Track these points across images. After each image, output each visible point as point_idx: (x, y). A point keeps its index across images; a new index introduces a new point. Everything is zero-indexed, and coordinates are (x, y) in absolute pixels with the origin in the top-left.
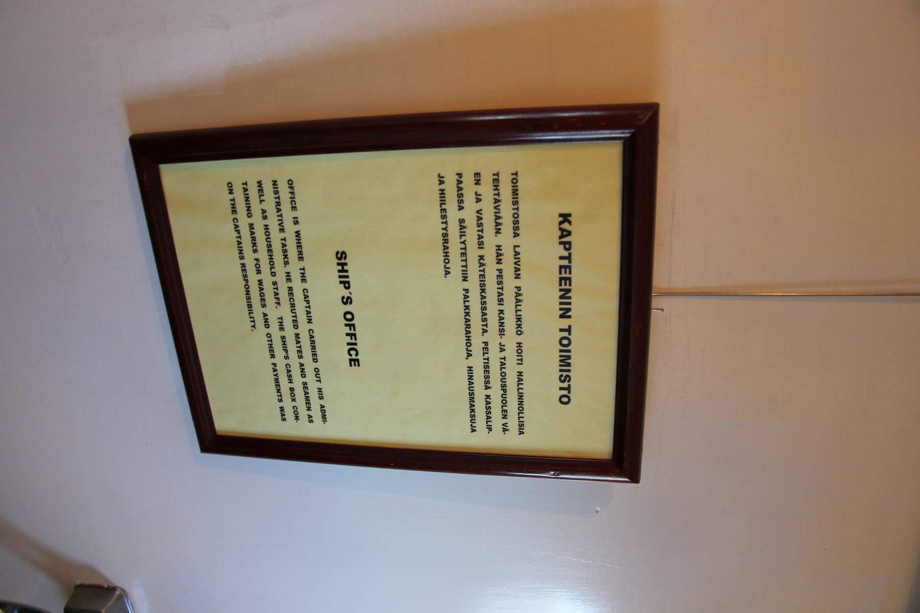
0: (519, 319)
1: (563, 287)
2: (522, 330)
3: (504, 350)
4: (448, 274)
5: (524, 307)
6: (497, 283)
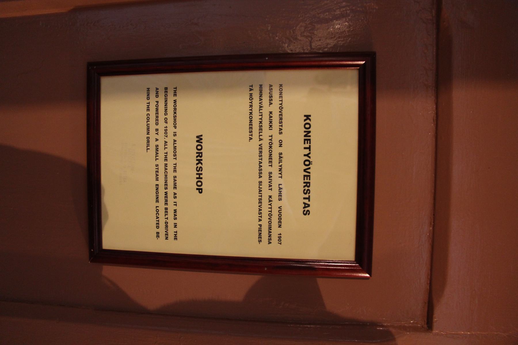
4: (271, 104)
6: (279, 200)
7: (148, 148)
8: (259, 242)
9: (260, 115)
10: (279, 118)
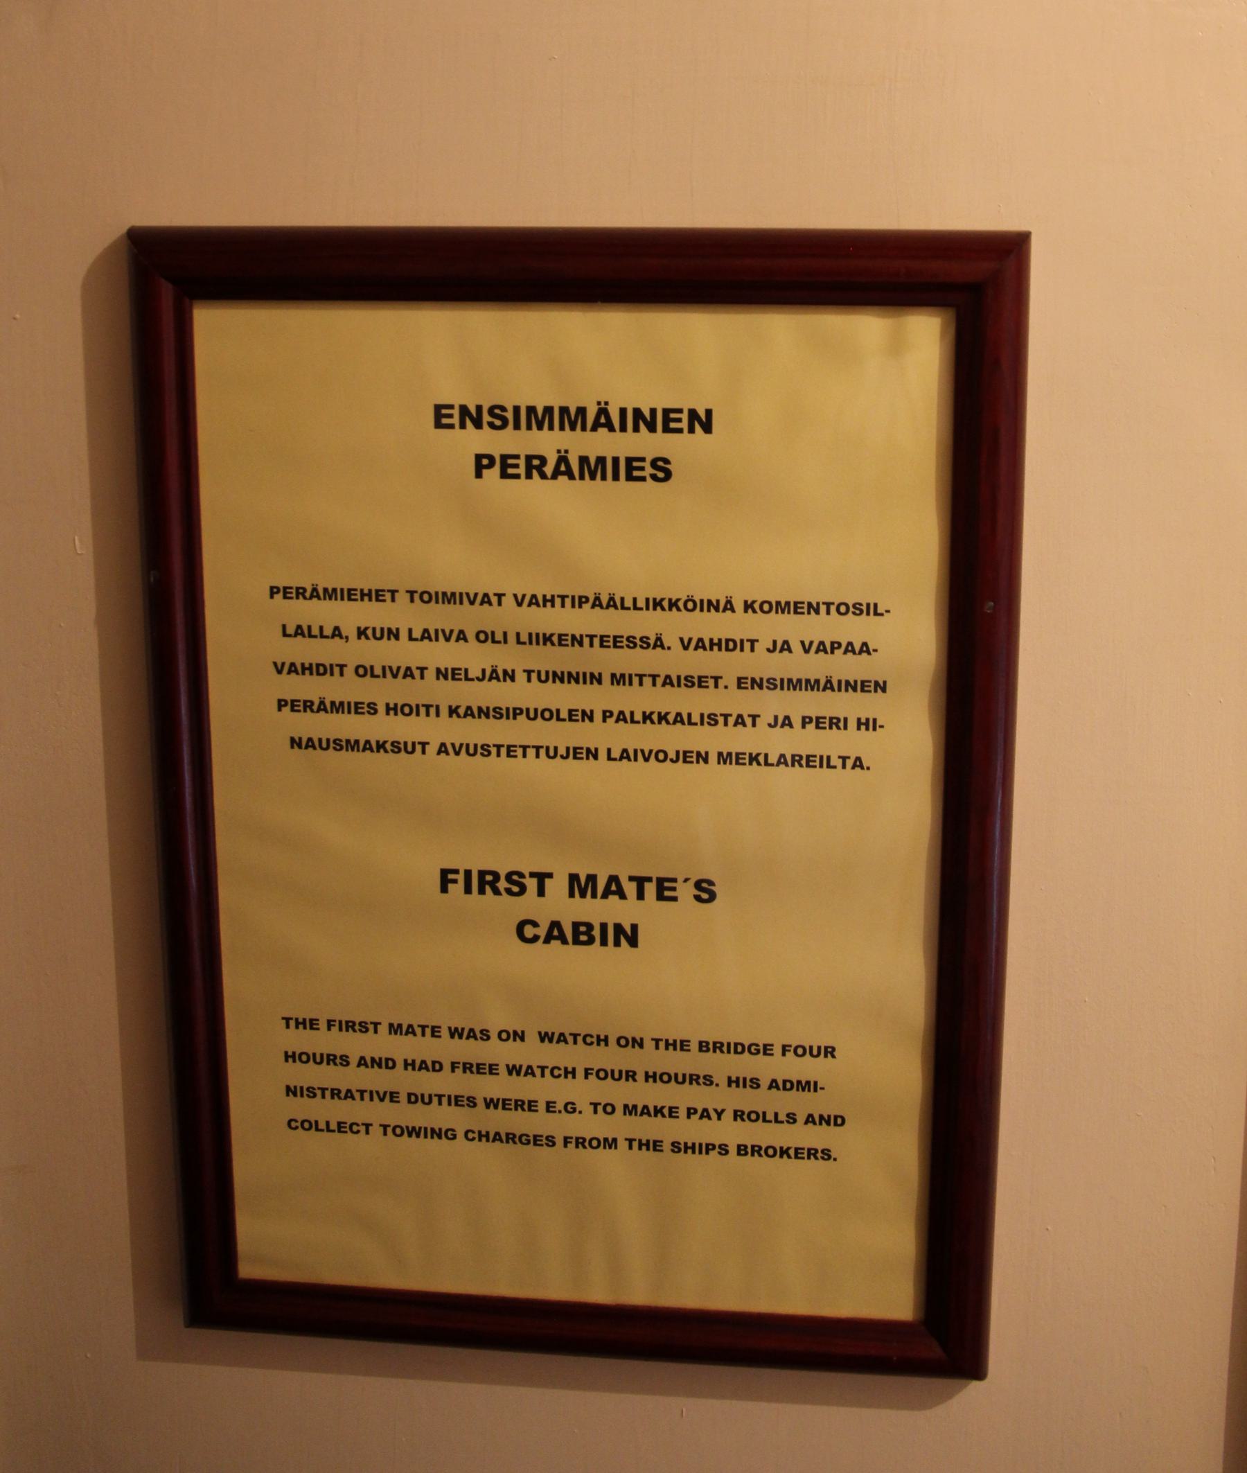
0: (658, 604)
1: (684, 425)
2: (684, 598)
3: (786, 642)
5: (625, 592)
7: (773, 1119)
8: (712, 1083)
9: (641, 684)
10: (809, 1158)
